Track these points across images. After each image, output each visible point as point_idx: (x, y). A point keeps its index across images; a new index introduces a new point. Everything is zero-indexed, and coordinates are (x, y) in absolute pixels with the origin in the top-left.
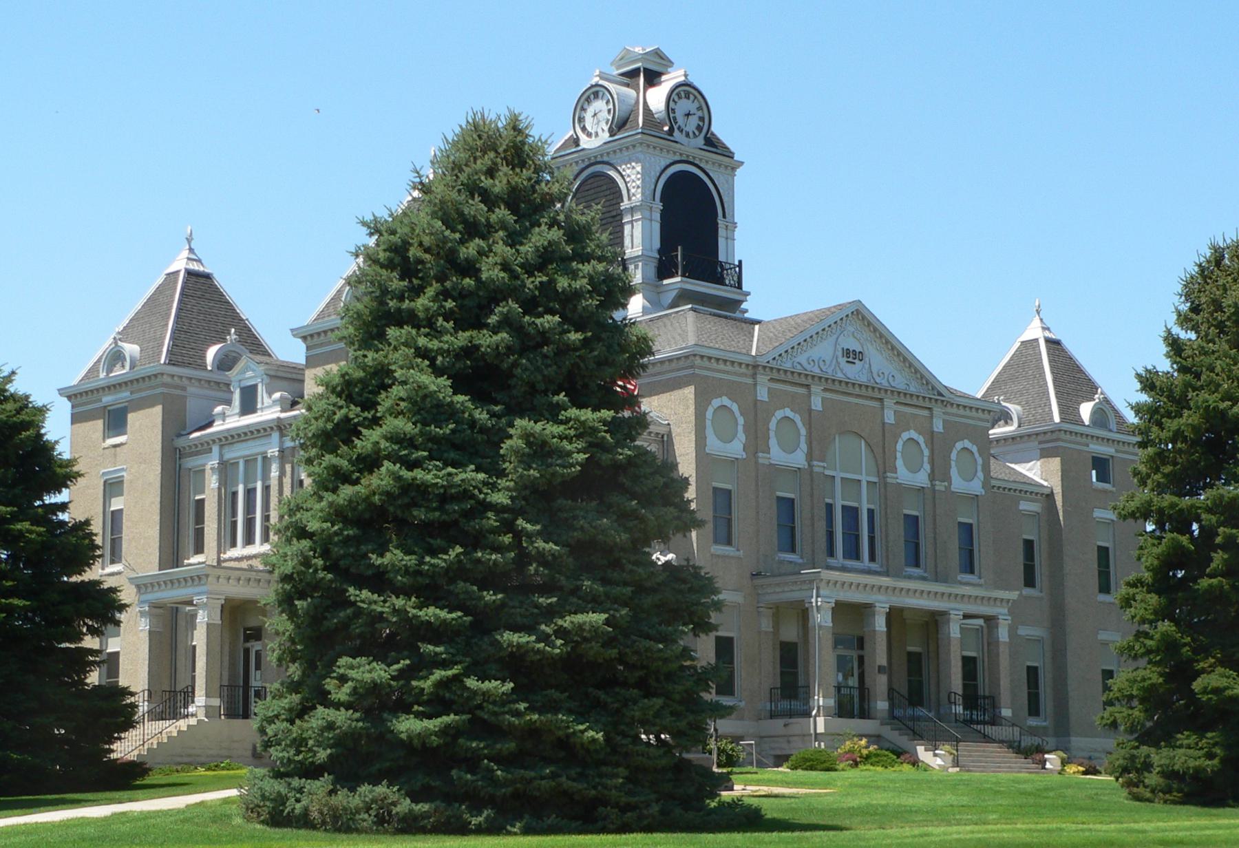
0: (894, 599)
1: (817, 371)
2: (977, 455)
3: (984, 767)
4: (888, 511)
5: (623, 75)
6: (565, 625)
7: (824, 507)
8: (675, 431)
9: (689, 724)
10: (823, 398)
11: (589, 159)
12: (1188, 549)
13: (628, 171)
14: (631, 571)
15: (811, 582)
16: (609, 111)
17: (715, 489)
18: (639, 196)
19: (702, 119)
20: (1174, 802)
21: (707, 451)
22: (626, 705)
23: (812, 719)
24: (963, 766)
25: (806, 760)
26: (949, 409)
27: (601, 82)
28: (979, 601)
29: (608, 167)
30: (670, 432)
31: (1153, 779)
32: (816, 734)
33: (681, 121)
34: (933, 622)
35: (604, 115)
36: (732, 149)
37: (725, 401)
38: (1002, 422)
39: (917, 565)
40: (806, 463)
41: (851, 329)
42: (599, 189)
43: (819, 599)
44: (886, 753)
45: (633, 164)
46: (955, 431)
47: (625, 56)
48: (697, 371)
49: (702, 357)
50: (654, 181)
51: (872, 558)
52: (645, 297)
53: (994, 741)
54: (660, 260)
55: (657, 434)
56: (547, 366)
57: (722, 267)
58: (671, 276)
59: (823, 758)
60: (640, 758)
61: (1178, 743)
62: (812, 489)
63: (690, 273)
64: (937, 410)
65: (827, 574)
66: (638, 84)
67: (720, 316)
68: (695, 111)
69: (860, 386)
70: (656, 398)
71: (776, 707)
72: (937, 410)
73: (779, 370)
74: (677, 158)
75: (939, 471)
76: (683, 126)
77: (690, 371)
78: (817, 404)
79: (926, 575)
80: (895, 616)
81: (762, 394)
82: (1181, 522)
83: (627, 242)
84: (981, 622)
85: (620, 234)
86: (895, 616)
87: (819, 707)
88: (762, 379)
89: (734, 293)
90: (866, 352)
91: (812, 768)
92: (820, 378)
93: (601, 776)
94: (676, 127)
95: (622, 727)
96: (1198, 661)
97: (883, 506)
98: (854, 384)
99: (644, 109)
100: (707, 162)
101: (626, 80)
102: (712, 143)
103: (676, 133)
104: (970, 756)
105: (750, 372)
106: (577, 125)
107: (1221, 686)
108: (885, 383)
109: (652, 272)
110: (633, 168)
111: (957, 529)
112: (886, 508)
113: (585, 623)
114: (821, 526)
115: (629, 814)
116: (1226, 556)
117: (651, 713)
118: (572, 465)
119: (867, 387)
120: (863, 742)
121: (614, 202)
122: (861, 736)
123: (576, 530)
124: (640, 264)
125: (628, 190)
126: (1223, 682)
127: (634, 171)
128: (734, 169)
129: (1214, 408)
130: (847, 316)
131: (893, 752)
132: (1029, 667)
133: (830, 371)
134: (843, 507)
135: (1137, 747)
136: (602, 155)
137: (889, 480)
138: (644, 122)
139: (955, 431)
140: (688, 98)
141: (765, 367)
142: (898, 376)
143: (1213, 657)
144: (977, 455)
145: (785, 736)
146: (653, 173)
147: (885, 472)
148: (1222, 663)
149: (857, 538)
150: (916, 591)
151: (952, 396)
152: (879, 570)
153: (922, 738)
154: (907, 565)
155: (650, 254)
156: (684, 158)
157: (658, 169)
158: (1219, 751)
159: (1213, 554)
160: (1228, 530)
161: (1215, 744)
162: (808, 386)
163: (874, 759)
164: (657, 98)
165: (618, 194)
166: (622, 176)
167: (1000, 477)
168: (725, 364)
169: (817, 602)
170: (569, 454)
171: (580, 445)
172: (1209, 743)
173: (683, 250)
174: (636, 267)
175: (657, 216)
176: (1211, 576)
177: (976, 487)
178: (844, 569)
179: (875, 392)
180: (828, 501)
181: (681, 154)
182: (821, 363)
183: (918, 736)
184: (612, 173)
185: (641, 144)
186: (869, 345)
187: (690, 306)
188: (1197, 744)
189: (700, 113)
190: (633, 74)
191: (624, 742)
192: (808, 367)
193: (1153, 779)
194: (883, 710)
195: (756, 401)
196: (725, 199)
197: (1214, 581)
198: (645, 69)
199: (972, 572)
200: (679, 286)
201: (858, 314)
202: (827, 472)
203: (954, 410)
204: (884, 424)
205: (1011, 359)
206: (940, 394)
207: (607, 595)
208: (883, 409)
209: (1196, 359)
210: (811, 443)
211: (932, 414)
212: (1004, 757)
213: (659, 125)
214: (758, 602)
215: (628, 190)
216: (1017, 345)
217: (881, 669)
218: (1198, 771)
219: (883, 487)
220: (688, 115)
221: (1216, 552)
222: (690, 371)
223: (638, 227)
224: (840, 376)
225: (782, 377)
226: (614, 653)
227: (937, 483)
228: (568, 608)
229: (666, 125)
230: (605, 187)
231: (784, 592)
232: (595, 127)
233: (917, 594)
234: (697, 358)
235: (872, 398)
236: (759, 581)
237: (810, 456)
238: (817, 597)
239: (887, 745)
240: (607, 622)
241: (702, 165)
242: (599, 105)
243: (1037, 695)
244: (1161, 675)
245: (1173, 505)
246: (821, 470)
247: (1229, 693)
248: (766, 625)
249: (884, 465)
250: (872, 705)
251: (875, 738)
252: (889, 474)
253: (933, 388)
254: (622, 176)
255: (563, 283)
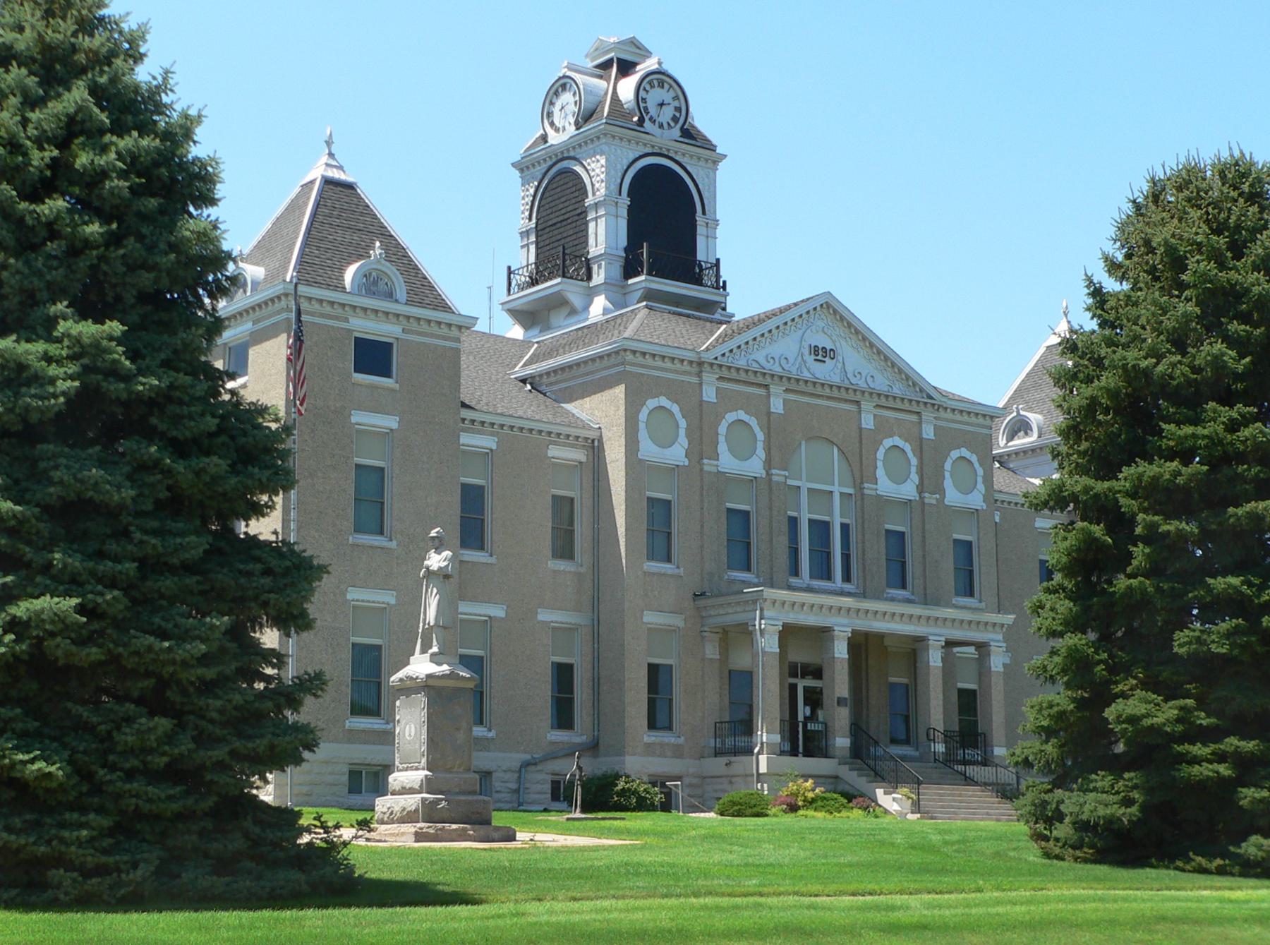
0: (858, 622)
1: (777, 369)
2: (977, 465)
3: (954, 813)
4: (866, 526)
5: (598, 66)
6: (19, 614)
7: (786, 520)
8: (606, 434)
9: (232, 753)
10: (784, 400)
11: (556, 155)
12: (1104, 544)
13: (593, 165)
14: (142, 542)
15: (755, 602)
16: (576, 102)
17: (650, 500)
18: (603, 191)
19: (678, 109)
20: (1085, 861)
21: (640, 457)
22: (118, 728)
23: (754, 757)
24: (927, 813)
25: (734, 804)
26: (942, 414)
27: (569, 73)
28: (965, 625)
29: (574, 162)
30: (601, 436)
31: (1063, 830)
32: (758, 774)
33: (653, 111)
34: (914, 648)
35: (572, 108)
36: (714, 142)
37: (663, 401)
38: (1022, 433)
39: (903, 586)
40: (764, 472)
41: (821, 324)
42: (565, 187)
43: (763, 622)
44: (835, 796)
45: (598, 157)
46: (948, 439)
47: (600, 48)
48: (628, 368)
49: (634, 352)
50: (620, 175)
51: (847, 578)
52: (607, 298)
53: (976, 784)
54: (627, 259)
55: (586, 439)
56: (51, 268)
57: (700, 266)
58: (637, 274)
59: (753, 802)
60: (134, 800)
61: (1091, 786)
62: (771, 499)
63: (658, 270)
64: (928, 415)
65: (771, 593)
66: (610, 76)
67: (680, 314)
68: (671, 101)
69: (831, 386)
70: (587, 399)
71: (723, 743)
72: (928, 415)
73: (730, 368)
74: (649, 150)
75: (930, 480)
76: (655, 117)
77: (621, 368)
78: (777, 405)
79: (913, 597)
80: (862, 645)
81: (709, 394)
82: (1100, 509)
83: (591, 241)
84: (972, 649)
85: (584, 233)
86: (862, 645)
87: (762, 744)
88: (709, 378)
89: (713, 293)
90: (839, 351)
91: (739, 814)
92: (781, 377)
93: (63, 825)
94: (647, 119)
95: (111, 758)
96: (1116, 683)
97: (860, 521)
98: (823, 385)
99: (612, 98)
100: (676, 153)
101: (599, 72)
102: (690, 134)
103: (647, 124)
104: (941, 801)
105: (695, 369)
106: (546, 121)
107: (1138, 713)
108: (862, 384)
109: (617, 270)
110: (598, 161)
111: (1038, 565)
112: (863, 522)
113: (43, 610)
114: (782, 541)
115: (94, 880)
116: (1147, 550)
117: (153, 737)
118: (55, 396)
119: (839, 388)
120: (809, 784)
121: (579, 199)
122: (806, 777)
123: (52, 483)
124: (603, 263)
125: (593, 185)
126: (1141, 709)
127: (599, 165)
128: (715, 163)
129: (1134, 366)
130: (815, 309)
131: (844, 795)
132: (650, 665)
133: (794, 370)
134: (810, 520)
135: (1050, 791)
136: (568, 150)
137: (866, 492)
138: (609, 112)
139: (948, 439)
140: (663, 87)
141: (712, 365)
142: (878, 377)
143: (1135, 678)
144: (977, 465)
145: (727, 776)
146: (619, 167)
147: (862, 483)
148: (1145, 685)
149: (828, 556)
150: (885, 613)
151: (943, 399)
152: (853, 591)
153: (883, 779)
154: (889, 585)
155: (614, 252)
156: (656, 150)
157: (626, 163)
158: (1137, 796)
159: (1132, 548)
160: (1149, 518)
161: (1135, 787)
162: (766, 387)
163: (820, 803)
164: (627, 89)
165: (582, 191)
166: (587, 170)
167: (1012, 491)
168: (663, 361)
169: (760, 624)
170: (52, 381)
171: (72, 368)
172: (1126, 786)
173: (649, 247)
174: (599, 267)
175: (624, 212)
176: (1129, 576)
177: (976, 500)
178: (809, 589)
179: (851, 394)
180: (790, 513)
181: (653, 147)
182: (783, 362)
183: (879, 776)
184: (578, 169)
185: (605, 135)
186: (844, 343)
187: (644, 303)
188: (1112, 786)
189: (676, 103)
190: (606, 66)
191: (114, 777)
192: (768, 366)
193: (1063, 830)
194: (843, 748)
195: (701, 402)
196: (705, 195)
197: (1134, 582)
198: (618, 59)
199: (971, 594)
200: (643, 285)
201: (828, 308)
202: (790, 482)
203: (949, 415)
204: (861, 429)
205: (1036, 365)
206: (930, 397)
207: (92, 573)
208: (860, 412)
209: (1120, 310)
210: (769, 449)
211: (921, 419)
212: (984, 802)
213: (627, 115)
214: (703, 626)
215: (593, 185)
216: (1043, 350)
217: (841, 702)
218: (1110, 821)
219: (859, 499)
220: (662, 105)
221: (1136, 545)
222: (621, 368)
223: (602, 222)
224: (806, 375)
225: (734, 375)
226: (94, 653)
227: (926, 495)
228: (29, 590)
229: (635, 115)
230: (571, 184)
231: (736, 613)
232: (562, 121)
233: (939, 622)
234: (628, 353)
235: (846, 401)
236: (702, 602)
237: (768, 464)
238: (761, 619)
239: (840, 788)
240: (80, 609)
241: (677, 158)
242: (567, 98)
243: (570, 701)
244: (1074, 700)
245: (1087, 490)
246: (782, 479)
247: (1147, 722)
248: (711, 651)
249: (861, 473)
250: (830, 743)
251: (832, 781)
252: (866, 485)
253: (921, 390)
254: (587, 170)
255: (83, 160)
